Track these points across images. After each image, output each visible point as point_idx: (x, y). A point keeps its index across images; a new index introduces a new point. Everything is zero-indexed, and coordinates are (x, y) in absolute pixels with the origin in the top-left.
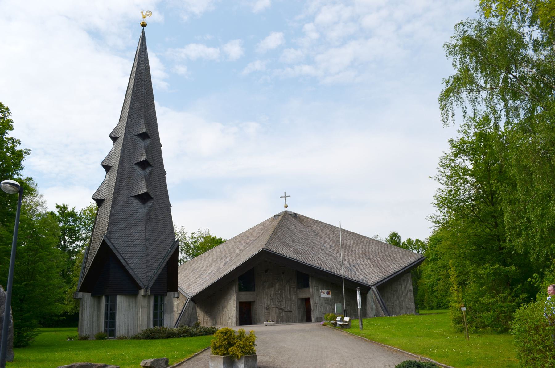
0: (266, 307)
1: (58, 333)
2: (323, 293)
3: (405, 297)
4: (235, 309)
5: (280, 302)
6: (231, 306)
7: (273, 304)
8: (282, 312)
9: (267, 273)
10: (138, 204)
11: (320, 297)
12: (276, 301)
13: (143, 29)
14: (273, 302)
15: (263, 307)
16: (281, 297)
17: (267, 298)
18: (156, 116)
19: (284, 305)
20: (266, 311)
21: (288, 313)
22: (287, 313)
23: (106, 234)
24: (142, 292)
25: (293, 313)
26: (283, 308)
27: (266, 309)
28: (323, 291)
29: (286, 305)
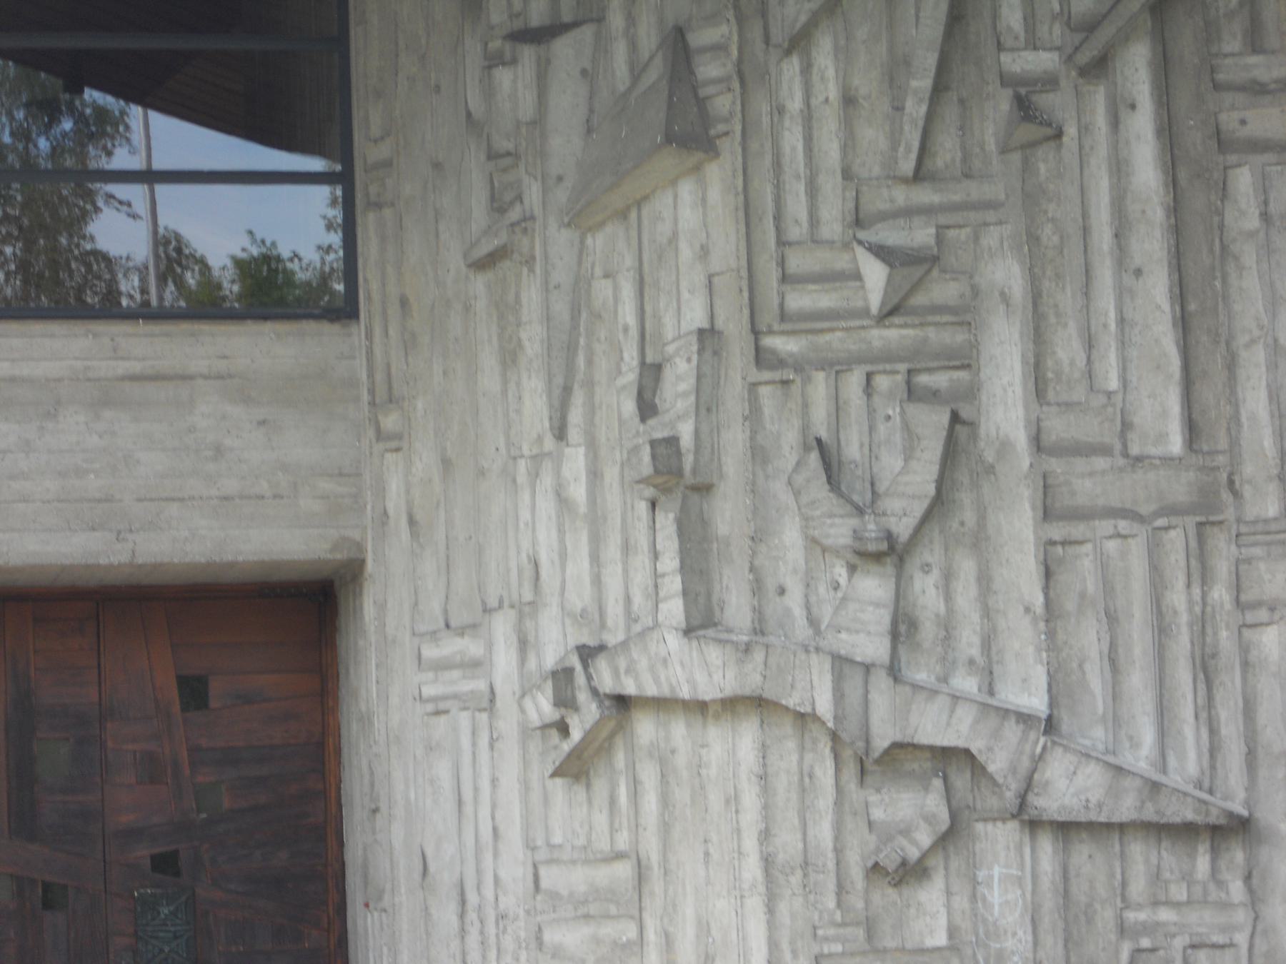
12: (791, 536)
17: (575, 460)
22: (1084, 855)
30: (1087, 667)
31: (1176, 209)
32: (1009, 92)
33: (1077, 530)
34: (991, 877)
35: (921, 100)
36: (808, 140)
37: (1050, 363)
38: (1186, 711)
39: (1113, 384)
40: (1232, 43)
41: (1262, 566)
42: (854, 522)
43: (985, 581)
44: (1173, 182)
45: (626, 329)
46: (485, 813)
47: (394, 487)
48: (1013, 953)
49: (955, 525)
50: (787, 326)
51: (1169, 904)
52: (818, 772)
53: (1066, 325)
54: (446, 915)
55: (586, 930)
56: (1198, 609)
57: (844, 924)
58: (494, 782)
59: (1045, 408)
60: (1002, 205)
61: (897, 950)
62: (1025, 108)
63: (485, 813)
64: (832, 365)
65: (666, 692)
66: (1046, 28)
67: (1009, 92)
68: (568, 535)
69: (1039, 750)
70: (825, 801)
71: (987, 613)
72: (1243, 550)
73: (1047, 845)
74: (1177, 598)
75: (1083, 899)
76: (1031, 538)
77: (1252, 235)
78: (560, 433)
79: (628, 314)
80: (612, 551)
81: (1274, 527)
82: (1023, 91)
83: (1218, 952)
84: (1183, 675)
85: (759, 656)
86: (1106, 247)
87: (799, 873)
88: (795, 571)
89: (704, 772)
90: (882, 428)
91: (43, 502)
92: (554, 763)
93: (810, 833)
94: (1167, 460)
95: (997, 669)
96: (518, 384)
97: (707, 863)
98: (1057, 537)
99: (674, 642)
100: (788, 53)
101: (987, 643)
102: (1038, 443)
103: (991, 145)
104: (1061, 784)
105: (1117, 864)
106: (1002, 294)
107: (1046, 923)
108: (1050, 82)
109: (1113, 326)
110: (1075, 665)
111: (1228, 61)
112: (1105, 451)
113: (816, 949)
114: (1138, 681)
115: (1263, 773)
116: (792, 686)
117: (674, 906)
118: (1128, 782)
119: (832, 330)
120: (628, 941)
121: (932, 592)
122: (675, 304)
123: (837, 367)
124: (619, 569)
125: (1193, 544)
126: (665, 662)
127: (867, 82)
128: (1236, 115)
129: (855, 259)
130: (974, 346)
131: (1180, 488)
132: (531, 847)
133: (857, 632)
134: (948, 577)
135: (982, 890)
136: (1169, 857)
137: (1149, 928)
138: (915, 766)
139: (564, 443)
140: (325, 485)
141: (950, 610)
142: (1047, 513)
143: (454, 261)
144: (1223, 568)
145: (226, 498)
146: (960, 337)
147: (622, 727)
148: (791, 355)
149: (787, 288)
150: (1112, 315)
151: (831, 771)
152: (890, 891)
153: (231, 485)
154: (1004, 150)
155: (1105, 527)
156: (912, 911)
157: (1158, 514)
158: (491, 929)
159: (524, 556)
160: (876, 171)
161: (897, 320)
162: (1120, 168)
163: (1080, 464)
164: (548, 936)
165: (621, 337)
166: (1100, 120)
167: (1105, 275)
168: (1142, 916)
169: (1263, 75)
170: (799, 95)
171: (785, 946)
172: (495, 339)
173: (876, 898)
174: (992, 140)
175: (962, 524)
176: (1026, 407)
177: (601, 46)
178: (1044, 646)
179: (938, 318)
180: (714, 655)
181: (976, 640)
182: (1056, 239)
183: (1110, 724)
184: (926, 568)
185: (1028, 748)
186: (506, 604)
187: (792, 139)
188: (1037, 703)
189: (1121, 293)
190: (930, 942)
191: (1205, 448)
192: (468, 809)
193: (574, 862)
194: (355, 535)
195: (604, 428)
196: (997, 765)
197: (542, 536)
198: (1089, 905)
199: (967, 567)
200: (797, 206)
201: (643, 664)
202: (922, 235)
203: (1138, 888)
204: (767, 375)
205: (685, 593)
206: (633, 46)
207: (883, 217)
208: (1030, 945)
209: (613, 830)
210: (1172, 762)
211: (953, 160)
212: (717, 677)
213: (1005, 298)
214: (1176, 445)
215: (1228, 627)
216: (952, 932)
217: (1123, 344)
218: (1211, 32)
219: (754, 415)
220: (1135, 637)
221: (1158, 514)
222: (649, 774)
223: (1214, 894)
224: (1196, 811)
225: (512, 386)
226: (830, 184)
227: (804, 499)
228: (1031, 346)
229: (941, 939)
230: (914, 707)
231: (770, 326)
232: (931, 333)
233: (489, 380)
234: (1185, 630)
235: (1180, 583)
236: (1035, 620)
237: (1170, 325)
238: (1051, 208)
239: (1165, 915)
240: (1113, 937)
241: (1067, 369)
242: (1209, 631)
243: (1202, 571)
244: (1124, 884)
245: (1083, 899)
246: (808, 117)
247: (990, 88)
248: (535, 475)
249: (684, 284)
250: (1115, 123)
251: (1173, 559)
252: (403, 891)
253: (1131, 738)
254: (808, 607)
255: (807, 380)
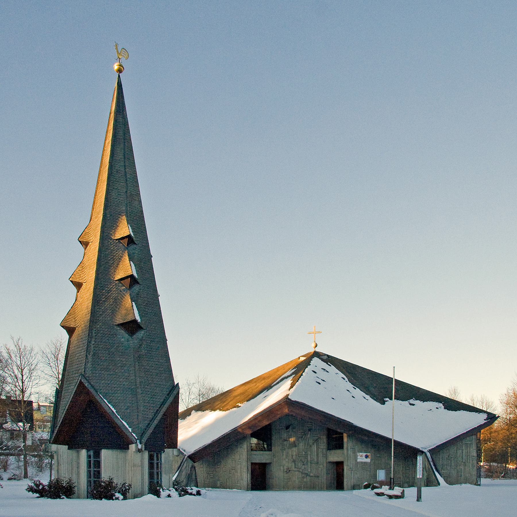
0: (285, 470)
2: (361, 456)
3: (466, 465)
4: (245, 470)
5: (304, 465)
6: (241, 468)
7: (295, 468)
10: (123, 335)
11: (356, 461)
13: (119, 76)
16: (306, 459)
18: (145, 227)
19: (309, 468)
20: (286, 475)
23: (83, 373)
24: (133, 447)
25: (320, 478)
26: (307, 472)
27: (285, 473)
28: (361, 454)
40: (319, 444)
78: (286, 458)
91: (189, 388)
92: (27, 369)
108: (312, 445)
248: (284, 460)
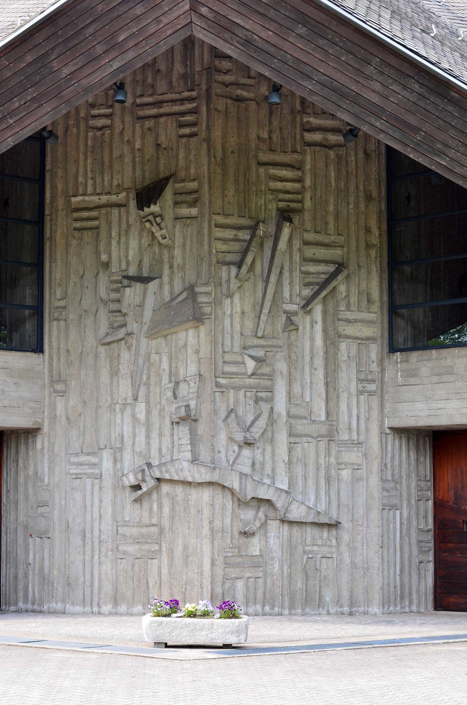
0: (132, 480)
1: (433, 58)
7: (194, 460)
8: (264, 525)
9: (154, 208)
12: (223, 437)
14: (193, 443)
15: (108, 482)
17: (141, 407)
19: (281, 469)
21: (310, 532)
22: (295, 530)
25: (346, 537)
27: (130, 496)
29: (299, 470)
30: (298, 478)
31: (326, 352)
32: (285, 315)
33: (298, 440)
34: (271, 536)
35: (265, 316)
36: (232, 323)
37: (292, 392)
38: (323, 492)
39: (308, 400)
40: (342, 308)
41: (343, 453)
42: (244, 434)
43: (273, 452)
44: (326, 345)
45: (164, 370)
46: (96, 509)
47: (60, 407)
48: (276, 557)
49: (266, 436)
50: (224, 376)
51: (317, 545)
52: (227, 504)
53: (297, 382)
54: (76, 540)
55: (137, 547)
56: (327, 464)
57: (232, 548)
58: (101, 501)
59: (291, 405)
60: (282, 347)
61: (246, 556)
62: (289, 319)
63: (96, 509)
64: (236, 388)
65: (182, 479)
66: (295, 298)
67: (285, 315)
68: (137, 429)
69: (290, 501)
70: (228, 513)
71: (274, 461)
72: (339, 448)
73: (286, 527)
74: (322, 460)
75: (295, 543)
76: (286, 441)
77: (345, 361)
78: (136, 399)
79: (165, 365)
80: (155, 434)
81: (347, 443)
82: (289, 315)
83: (328, 559)
84: (322, 482)
85: (218, 471)
86: (308, 361)
87: (221, 533)
88: (223, 446)
89: (189, 502)
90: (248, 407)
93: (224, 521)
94: (321, 422)
95: (275, 477)
96: (118, 381)
97: (189, 529)
98: (293, 442)
99: (185, 465)
100: (227, 297)
101: (273, 470)
102: (289, 415)
103: (280, 330)
104: (295, 511)
105: (304, 534)
106: (280, 372)
107: (285, 549)
108: (296, 314)
109: (309, 383)
110: (295, 477)
111: (342, 312)
112: (305, 418)
113: (225, 555)
114: (311, 482)
115: (341, 510)
116: (227, 480)
117: (174, 540)
118: (312, 511)
119: (236, 378)
120: (154, 550)
121: (259, 454)
122: (185, 365)
123: (237, 388)
124: (157, 440)
125: (327, 446)
126: (181, 470)
127: (248, 308)
128: (343, 328)
129: (243, 357)
130: (273, 386)
131: (323, 430)
132: (115, 520)
133: (243, 465)
134: (264, 450)
135: (269, 539)
136: (316, 532)
137: (311, 552)
138: (253, 504)
139: (136, 401)
140: (32, 404)
141: (264, 460)
142: (291, 435)
143: (91, 341)
144: (333, 453)
145: (5, 407)
146: (269, 383)
147: (157, 488)
148: (224, 384)
149: (225, 365)
150: (309, 380)
151: (231, 504)
152: (245, 539)
153: (6, 403)
154: (283, 332)
155: (305, 439)
156: (250, 544)
157: (318, 437)
158: (96, 545)
159: (117, 434)
160: (249, 334)
161: (254, 377)
162: (312, 339)
163: (299, 421)
164: (120, 548)
165: (162, 372)
166: (308, 326)
167: (307, 369)
168: (309, 548)
169: (350, 317)
170: (229, 310)
171: (216, 554)
172: (108, 367)
173: (241, 540)
174: (280, 328)
175: (268, 436)
176: (286, 404)
177: (161, 286)
178: (288, 472)
179: (264, 377)
180: (203, 469)
181: (270, 469)
182: (295, 358)
183: (304, 494)
184: (258, 448)
185: (287, 500)
186: (108, 447)
187: (227, 322)
188: (285, 487)
189: (311, 374)
190: (254, 554)
191: (330, 419)
192: (89, 508)
193: (134, 526)
194: (39, 420)
195: (153, 398)
196: (279, 505)
197: (125, 428)
198: (296, 545)
199: (269, 448)
200: (228, 341)
201: (172, 470)
202: (260, 353)
203: (309, 540)
204: (218, 390)
205: (191, 451)
206: (172, 287)
207: (251, 347)
208: (281, 555)
209: (151, 518)
210: (318, 506)
211: (270, 333)
212: (203, 476)
213: (281, 373)
214: (323, 418)
215: (334, 469)
216: (261, 551)
217: (311, 389)
218: (337, 305)
219: (214, 401)
220: (311, 470)
221: (318, 437)
222: (166, 503)
223: (328, 543)
224: (329, 520)
225: (115, 383)
226: (237, 336)
227: (230, 427)
228: (288, 387)
229: (257, 553)
230: (258, 487)
231: (219, 375)
232: (262, 381)
233: (105, 378)
234: (323, 469)
235: (323, 456)
236: (285, 464)
237: (323, 385)
238: (295, 348)
239: (315, 548)
240: (302, 554)
241: (296, 394)
242: (329, 470)
243: (328, 453)
244: (305, 539)
245: (295, 543)
246: (231, 316)
247: (280, 313)
249: (189, 360)
250: (312, 327)
251: (321, 449)
252: (57, 532)
253: (308, 498)
254: (227, 457)
255: (229, 392)
